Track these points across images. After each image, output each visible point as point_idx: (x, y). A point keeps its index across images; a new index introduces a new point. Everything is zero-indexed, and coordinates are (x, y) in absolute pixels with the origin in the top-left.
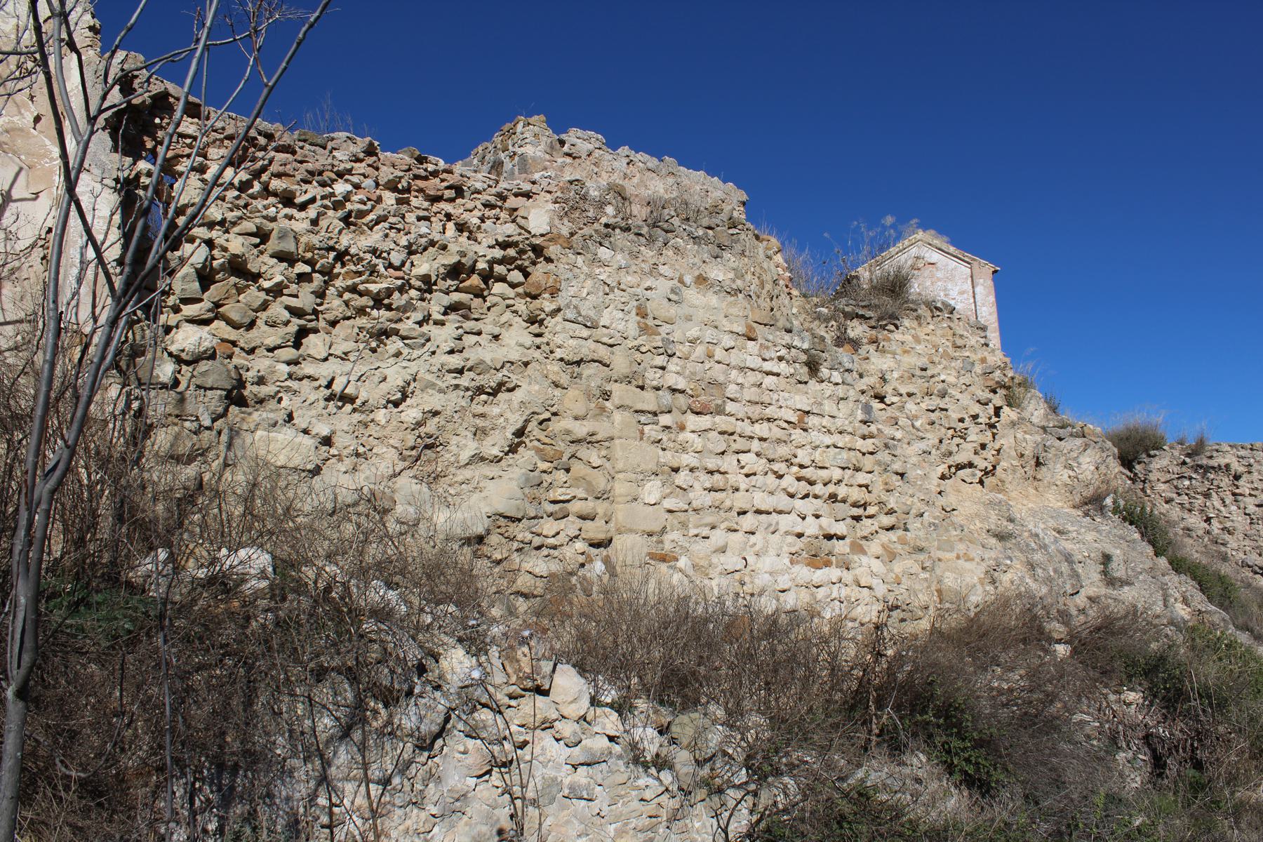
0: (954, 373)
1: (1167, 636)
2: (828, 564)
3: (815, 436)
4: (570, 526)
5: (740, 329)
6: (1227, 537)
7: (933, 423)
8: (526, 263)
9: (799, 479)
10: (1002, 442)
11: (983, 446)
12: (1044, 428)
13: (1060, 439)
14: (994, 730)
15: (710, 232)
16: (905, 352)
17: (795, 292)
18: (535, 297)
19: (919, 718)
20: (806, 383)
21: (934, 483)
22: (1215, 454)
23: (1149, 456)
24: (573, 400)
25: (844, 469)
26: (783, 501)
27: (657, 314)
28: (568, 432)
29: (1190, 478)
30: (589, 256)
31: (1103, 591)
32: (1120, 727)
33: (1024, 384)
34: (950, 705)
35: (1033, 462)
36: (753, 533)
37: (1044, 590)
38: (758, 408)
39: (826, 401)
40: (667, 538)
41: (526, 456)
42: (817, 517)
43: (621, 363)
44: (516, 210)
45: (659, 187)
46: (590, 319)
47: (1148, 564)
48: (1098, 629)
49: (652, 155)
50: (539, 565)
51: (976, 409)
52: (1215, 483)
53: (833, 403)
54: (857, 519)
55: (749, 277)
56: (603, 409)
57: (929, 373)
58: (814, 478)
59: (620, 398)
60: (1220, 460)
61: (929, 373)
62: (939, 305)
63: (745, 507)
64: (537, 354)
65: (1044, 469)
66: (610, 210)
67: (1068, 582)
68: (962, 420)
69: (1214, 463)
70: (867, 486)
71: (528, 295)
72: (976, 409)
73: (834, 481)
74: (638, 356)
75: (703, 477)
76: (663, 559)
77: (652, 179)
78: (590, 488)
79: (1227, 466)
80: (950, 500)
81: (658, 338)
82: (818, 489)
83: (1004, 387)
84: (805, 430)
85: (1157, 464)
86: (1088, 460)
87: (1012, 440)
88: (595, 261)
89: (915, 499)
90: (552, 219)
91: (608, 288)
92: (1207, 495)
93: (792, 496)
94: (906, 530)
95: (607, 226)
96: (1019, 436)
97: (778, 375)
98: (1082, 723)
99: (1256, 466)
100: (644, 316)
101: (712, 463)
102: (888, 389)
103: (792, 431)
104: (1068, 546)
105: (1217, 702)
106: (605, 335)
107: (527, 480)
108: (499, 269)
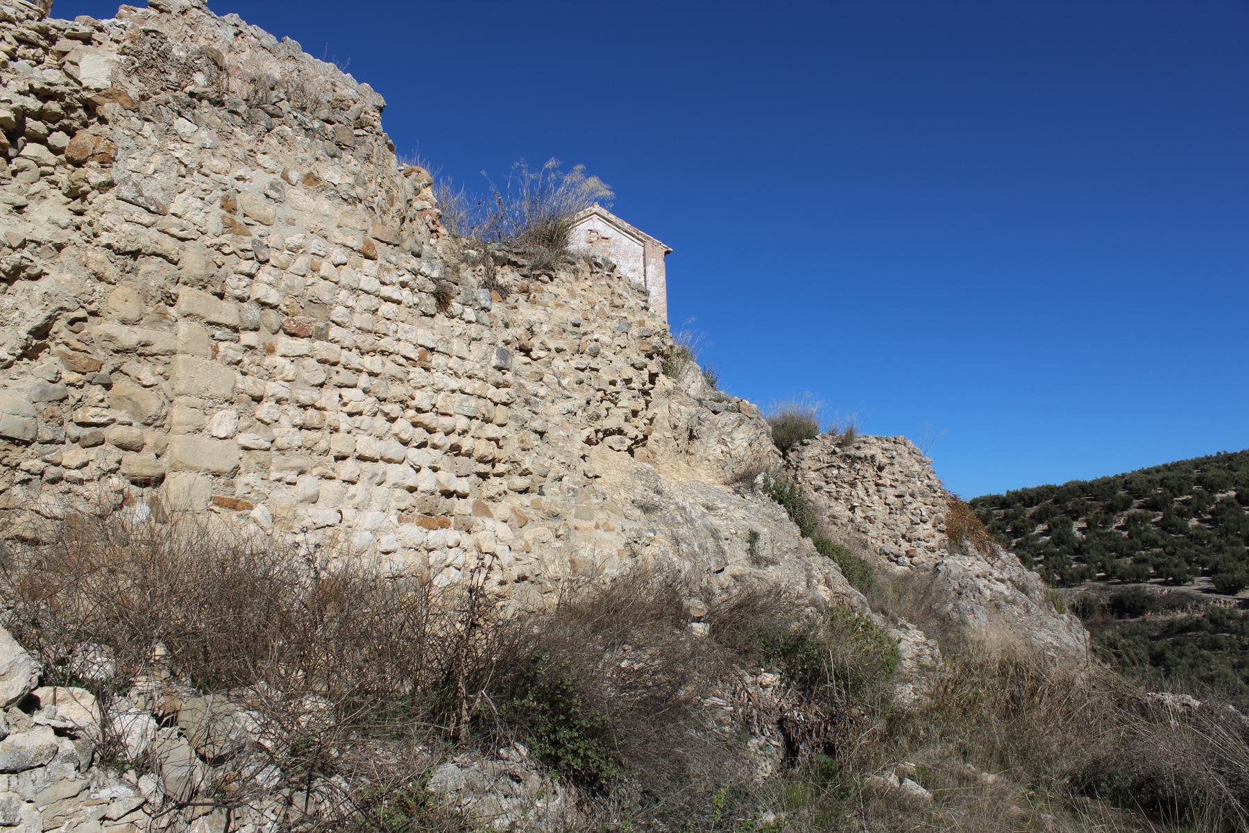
0: (609, 333)
1: (807, 617)
2: (444, 525)
3: (438, 378)
4: (107, 456)
5: (356, 243)
6: (868, 525)
7: (581, 382)
8: (76, 124)
9: (415, 425)
10: (655, 411)
11: (635, 413)
12: (700, 401)
13: (715, 413)
14: (607, 717)
15: (329, 127)
16: (558, 305)
17: (442, 230)
18: (79, 164)
19: (517, 703)
20: (432, 316)
21: (577, 446)
22: (862, 445)
23: (803, 444)
24: (121, 299)
25: (471, 418)
26: (395, 449)
27: (248, 210)
28: (111, 339)
29: (839, 468)
30: (162, 125)
31: (748, 570)
32: (755, 712)
33: (683, 354)
34: (557, 687)
35: (686, 435)
36: (353, 483)
37: (687, 566)
38: (371, 338)
39: (455, 340)
40: (240, 480)
41: (48, 362)
42: (435, 470)
43: (193, 261)
44: (64, 54)
45: (274, 69)
46: (156, 203)
47: (795, 544)
48: (739, 606)
49: (269, 31)
50: (49, 501)
51: (629, 373)
52: (861, 473)
53: (463, 347)
54: (484, 476)
55: (372, 187)
56: (164, 315)
57: (582, 330)
58: (433, 425)
59: (189, 304)
60: (866, 451)
61: (582, 330)
62: (599, 261)
63: (345, 450)
64: (76, 236)
65: (697, 443)
66: (200, 78)
67: (713, 559)
68: (613, 383)
69: (861, 454)
70: (497, 441)
71: (70, 160)
72: (629, 373)
73: (458, 430)
74: (219, 258)
75: (293, 411)
76: (233, 505)
77: (266, 59)
78: (136, 410)
79: (873, 457)
80: (595, 466)
81: (247, 239)
82: (438, 438)
83: (661, 354)
84: (427, 369)
85: (808, 452)
86: (742, 436)
87: (666, 410)
88: (169, 131)
89: (555, 462)
90: (114, 73)
91: (186, 170)
92: (853, 485)
93: (405, 443)
94: (541, 493)
95: (192, 95)
96: (673, 406)
97: (399, 303)
98: (715, 707)
99: (898, 459)
100: (232, 210)
101: (305, 396)
102: (535, 342)
103: (411, 369)
104: (716, 522)
105: (852, 683)
106: (175, 225)
107: (44, 392)
108: (31, 124)
